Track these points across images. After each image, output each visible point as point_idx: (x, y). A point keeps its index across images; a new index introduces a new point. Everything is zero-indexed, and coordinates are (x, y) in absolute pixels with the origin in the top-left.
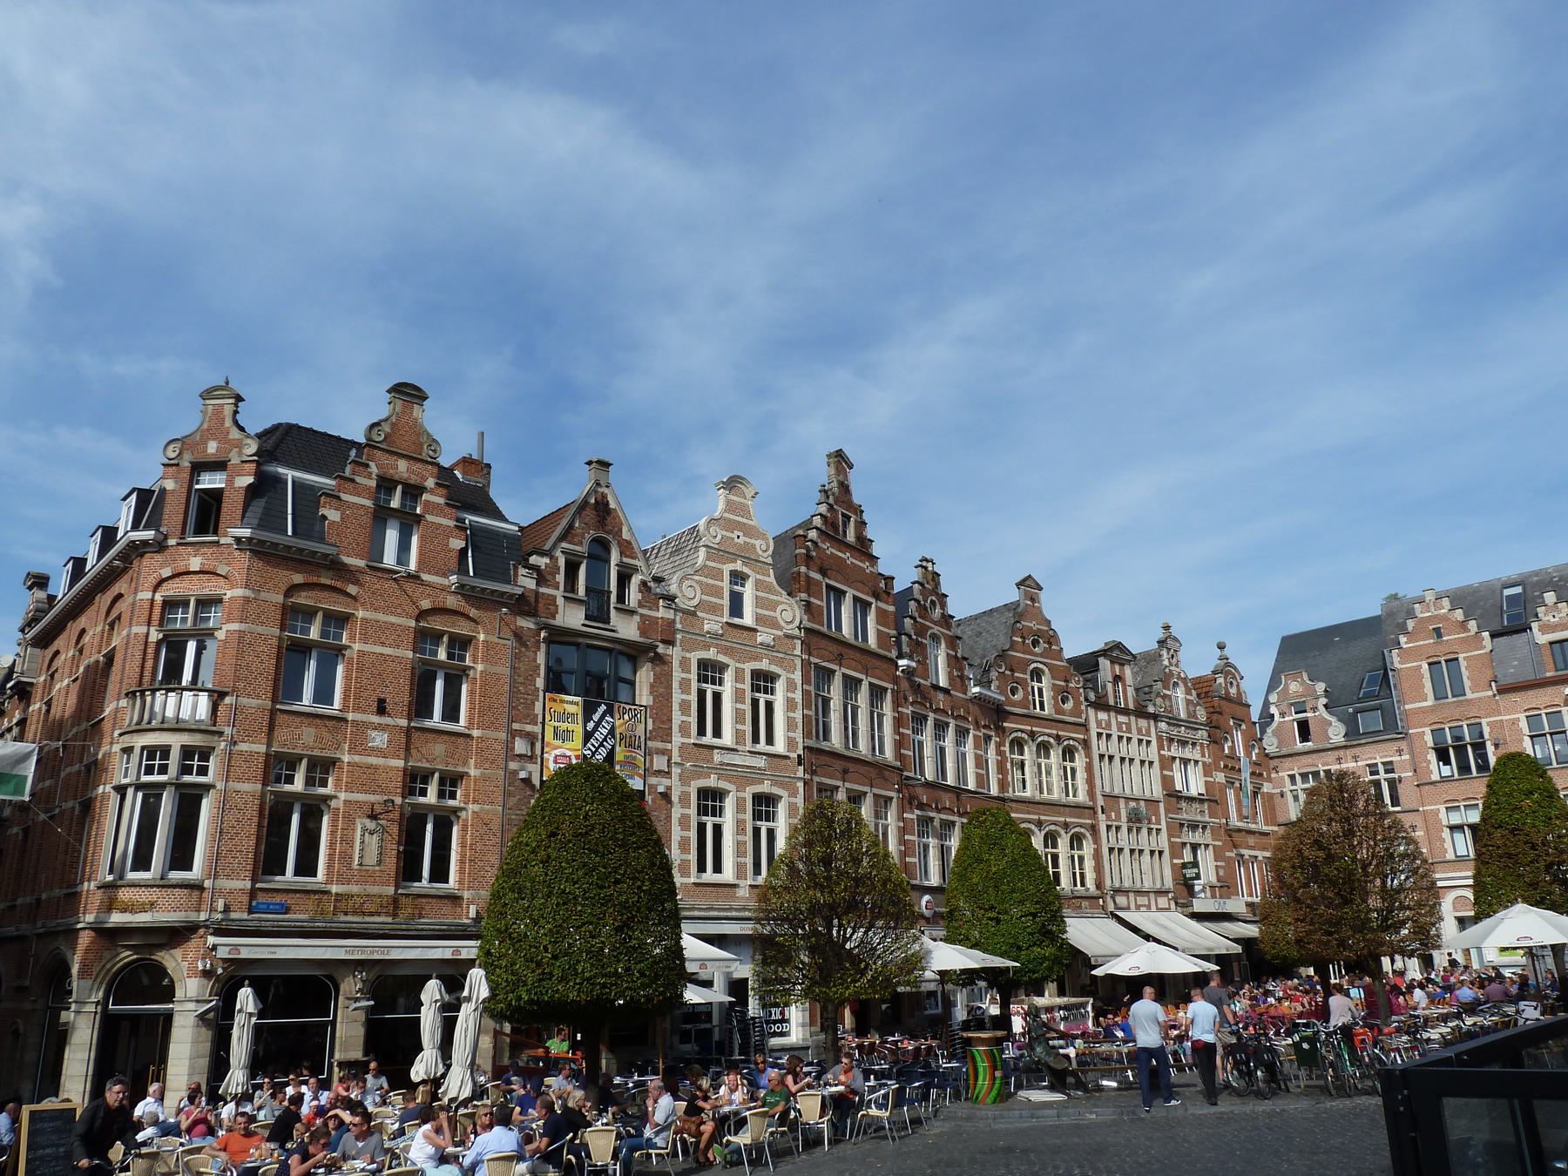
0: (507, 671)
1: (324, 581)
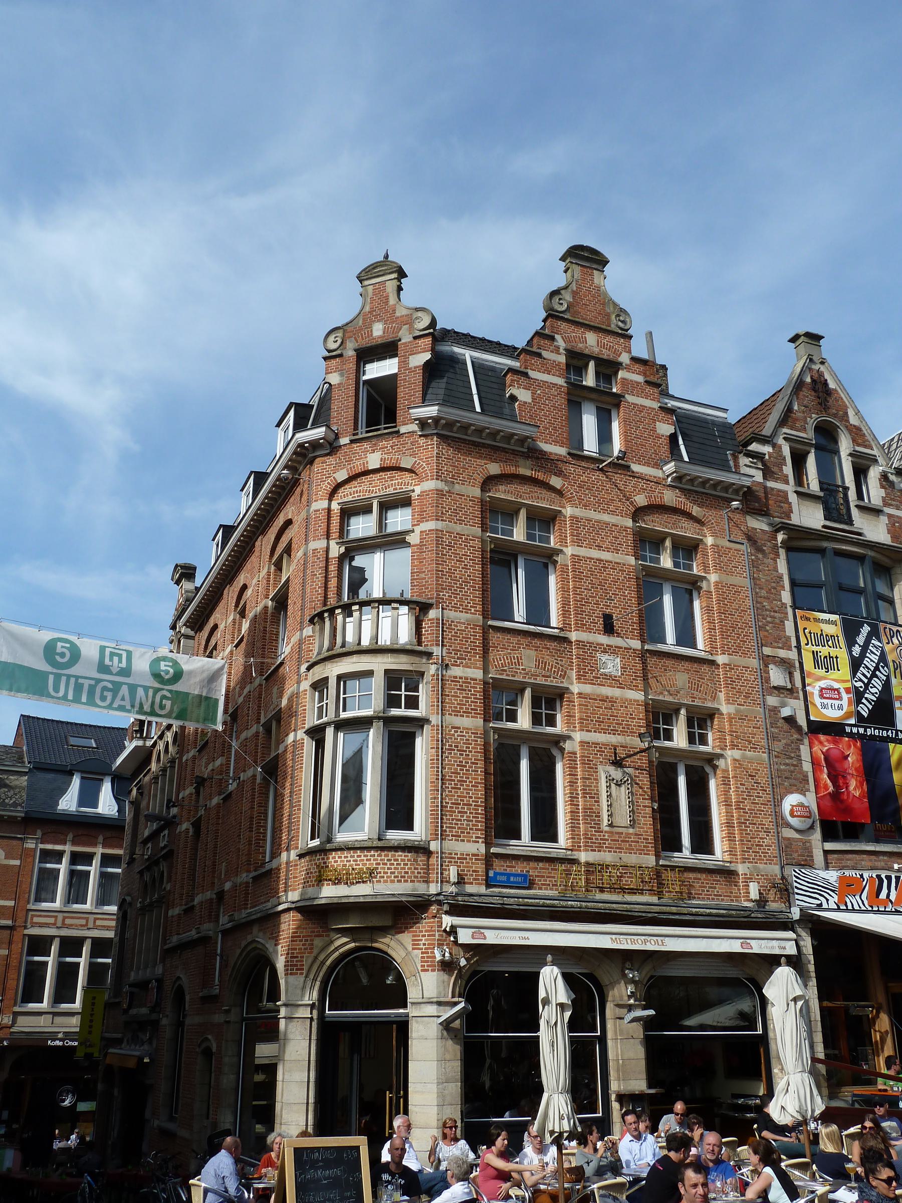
0: (747, 582)
1: (523, 471)
